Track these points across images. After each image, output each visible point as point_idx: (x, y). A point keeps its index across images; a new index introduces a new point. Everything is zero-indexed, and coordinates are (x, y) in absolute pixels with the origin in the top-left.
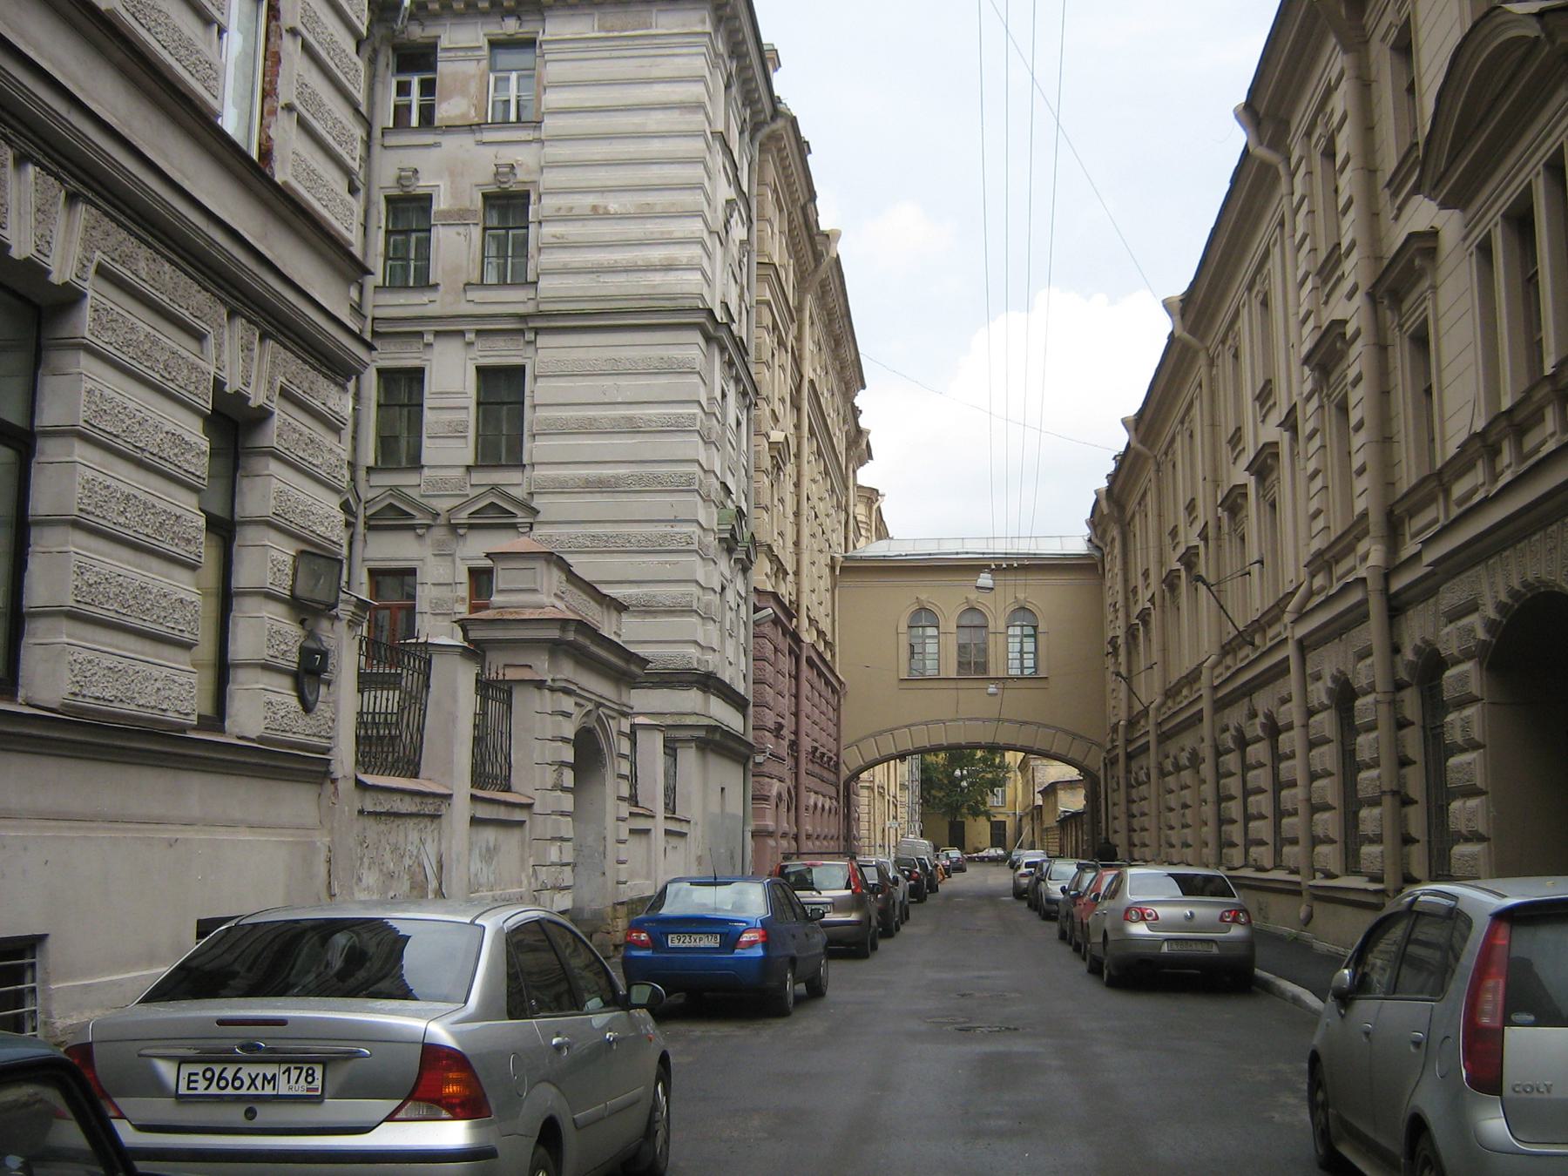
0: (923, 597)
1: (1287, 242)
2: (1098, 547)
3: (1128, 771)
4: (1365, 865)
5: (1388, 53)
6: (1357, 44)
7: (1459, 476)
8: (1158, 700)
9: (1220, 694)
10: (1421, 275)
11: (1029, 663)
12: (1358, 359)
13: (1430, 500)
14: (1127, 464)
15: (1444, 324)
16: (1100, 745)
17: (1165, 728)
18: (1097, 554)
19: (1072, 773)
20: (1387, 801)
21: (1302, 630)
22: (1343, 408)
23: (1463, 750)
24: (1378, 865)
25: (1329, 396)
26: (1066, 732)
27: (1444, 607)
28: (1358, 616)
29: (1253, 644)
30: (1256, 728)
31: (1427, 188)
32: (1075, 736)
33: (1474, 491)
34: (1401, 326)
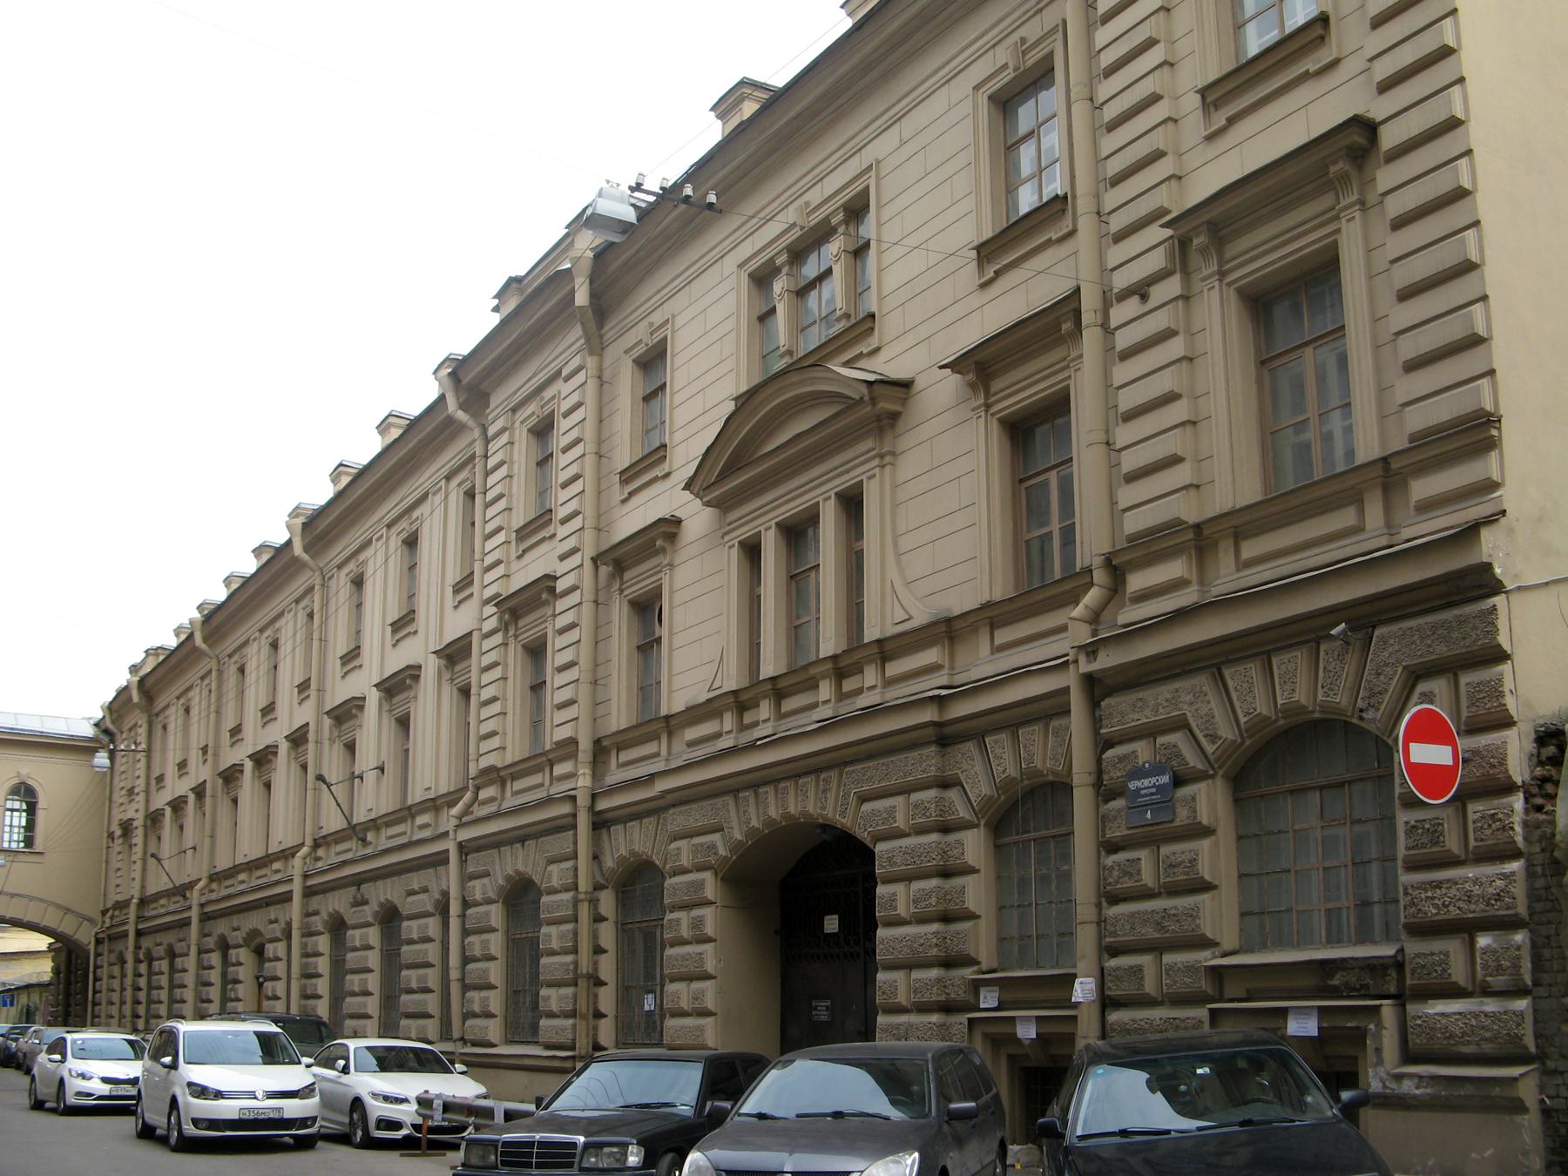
2: (106, 732)
3: (138, 947)
4: (544, 1037)
5: (630, 363)
6: (596, 345)
8: (202, 884)
9: (310, 883)
10: (663, 550)
13: (655, 737)
14: (174, 660)
15: (679, 597)
16: (91, 920)
17: (208, 909)
19: (41, 942)
20: (582, 983)
21: (464, 835)
22: (536, 651)
24: (570, 1036)
25: (516, 636)
26: (58, 906)
28: (568, 825)
29: (364, 840)
30: (160, 951)
32: (68, 910)
34: (621, 591)
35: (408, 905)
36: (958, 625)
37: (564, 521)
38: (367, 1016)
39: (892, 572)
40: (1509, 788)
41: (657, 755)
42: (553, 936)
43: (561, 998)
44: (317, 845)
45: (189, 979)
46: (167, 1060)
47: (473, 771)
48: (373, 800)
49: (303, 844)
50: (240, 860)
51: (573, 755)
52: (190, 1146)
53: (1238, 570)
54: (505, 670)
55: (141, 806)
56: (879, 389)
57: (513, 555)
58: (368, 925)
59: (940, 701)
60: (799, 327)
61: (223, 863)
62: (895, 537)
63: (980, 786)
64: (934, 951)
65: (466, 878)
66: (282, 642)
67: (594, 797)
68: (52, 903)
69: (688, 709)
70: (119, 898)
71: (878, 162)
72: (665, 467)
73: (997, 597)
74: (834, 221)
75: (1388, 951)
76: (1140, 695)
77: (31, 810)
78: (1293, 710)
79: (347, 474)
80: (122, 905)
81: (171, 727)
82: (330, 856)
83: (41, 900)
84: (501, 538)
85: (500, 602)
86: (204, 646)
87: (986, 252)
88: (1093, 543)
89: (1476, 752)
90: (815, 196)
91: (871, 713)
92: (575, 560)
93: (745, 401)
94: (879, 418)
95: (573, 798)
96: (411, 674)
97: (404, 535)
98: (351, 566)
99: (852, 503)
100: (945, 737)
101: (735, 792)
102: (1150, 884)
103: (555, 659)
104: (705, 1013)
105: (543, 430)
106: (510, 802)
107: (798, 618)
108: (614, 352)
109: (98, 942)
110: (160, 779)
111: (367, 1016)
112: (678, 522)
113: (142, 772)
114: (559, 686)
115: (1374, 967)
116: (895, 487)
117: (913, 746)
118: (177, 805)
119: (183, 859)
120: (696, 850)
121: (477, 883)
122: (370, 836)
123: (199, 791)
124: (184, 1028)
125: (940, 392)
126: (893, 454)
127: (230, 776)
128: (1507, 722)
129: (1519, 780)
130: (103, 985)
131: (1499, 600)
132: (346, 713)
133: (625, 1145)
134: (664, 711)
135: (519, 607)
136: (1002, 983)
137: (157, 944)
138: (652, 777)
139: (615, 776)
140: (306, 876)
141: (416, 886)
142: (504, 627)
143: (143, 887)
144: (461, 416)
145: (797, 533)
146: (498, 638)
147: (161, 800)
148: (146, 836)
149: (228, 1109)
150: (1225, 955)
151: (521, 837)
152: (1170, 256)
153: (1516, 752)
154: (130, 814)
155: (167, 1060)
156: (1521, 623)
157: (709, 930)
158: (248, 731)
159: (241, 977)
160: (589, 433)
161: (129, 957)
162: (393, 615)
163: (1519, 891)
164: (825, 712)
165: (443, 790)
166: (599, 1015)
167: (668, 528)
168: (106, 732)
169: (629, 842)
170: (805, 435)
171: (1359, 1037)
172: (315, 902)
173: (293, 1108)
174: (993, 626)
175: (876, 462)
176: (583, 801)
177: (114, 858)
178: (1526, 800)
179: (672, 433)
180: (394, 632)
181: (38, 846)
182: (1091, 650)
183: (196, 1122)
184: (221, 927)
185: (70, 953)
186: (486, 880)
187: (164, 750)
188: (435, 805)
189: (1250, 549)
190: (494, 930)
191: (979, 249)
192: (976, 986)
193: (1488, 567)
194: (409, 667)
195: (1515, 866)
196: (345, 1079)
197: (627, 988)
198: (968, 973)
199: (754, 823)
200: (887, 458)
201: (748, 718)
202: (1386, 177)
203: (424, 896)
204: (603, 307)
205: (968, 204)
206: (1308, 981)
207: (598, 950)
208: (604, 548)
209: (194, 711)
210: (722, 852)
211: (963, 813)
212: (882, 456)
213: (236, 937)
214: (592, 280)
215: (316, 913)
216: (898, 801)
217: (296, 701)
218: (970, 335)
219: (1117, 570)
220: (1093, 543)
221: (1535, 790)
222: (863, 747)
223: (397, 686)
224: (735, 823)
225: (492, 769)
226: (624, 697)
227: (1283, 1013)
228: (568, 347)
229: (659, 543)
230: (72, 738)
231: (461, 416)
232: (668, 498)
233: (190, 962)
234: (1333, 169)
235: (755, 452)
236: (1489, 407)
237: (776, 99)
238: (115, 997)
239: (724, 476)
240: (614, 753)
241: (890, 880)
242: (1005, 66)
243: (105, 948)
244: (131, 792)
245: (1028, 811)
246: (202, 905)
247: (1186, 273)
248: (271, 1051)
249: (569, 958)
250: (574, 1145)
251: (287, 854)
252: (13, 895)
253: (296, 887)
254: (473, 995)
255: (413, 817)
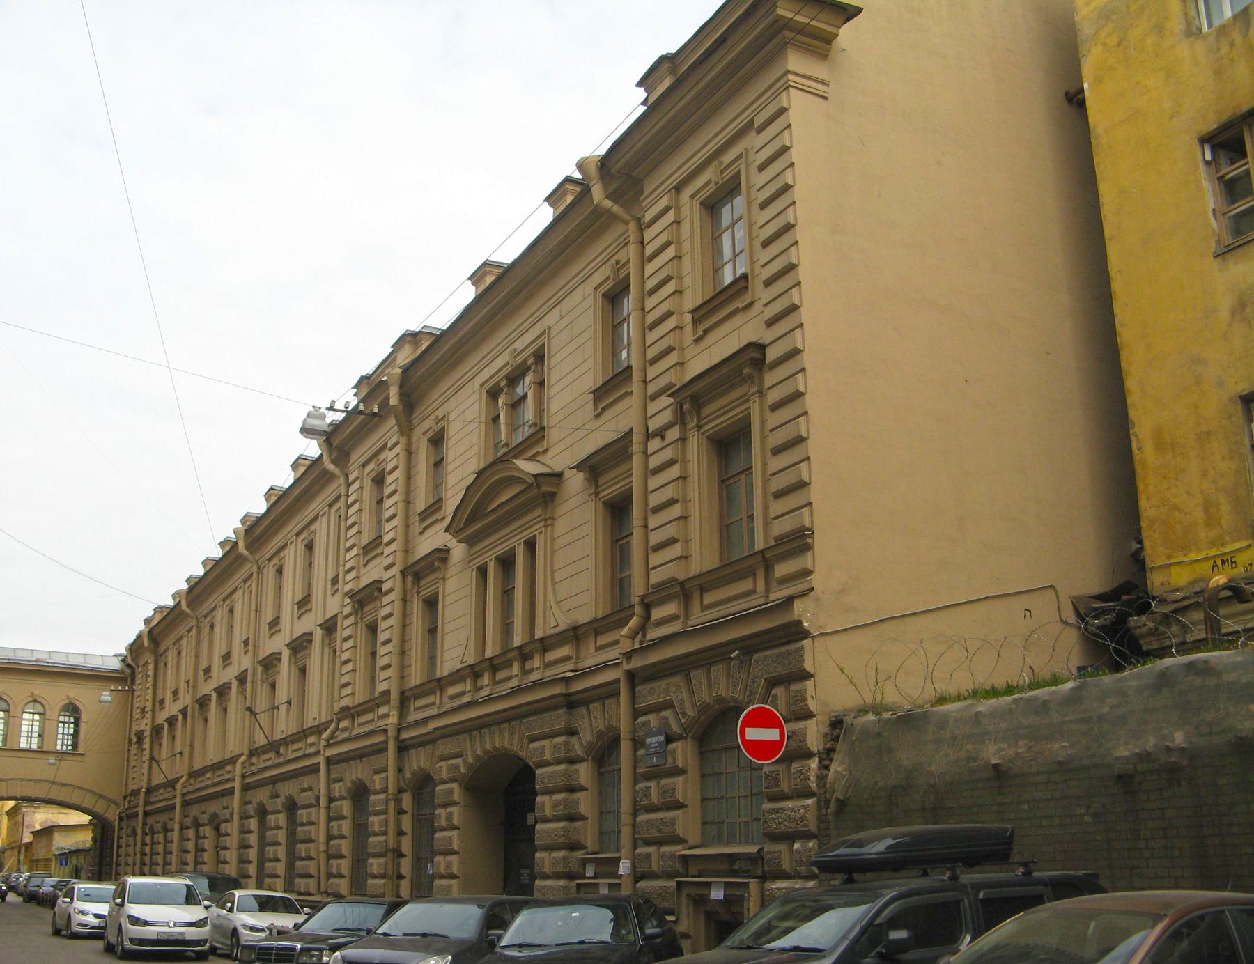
0: (36, 692)
1: (342, 523)
3: (145, 824)
4: (369, 891)
6: (406, 429)
7: (452, 683)
8: (184, 779)
9: (247, 781)
10: (439, 569)
11: (35, 741)
12: (389, 604)
13: (432, 692)
14: (170, 617)
15: (448, 600)
16: (116, 804)
17: (187, 798)
18: (128, 671)
19: (85, 819)
20: (390, 855)
21: (330, 752)
22: (373, 629)
23: (445, 830)
26: (93, 793)
27: (438, 753)
28: (381, 749)
29: (278, 752)
30: (158, 827)
31: (452, 530)
32: (100, 796)
33: (463, 693)
34: (418, 593)
35: (304, 798)
36: (580, 632)
37: (388, 544)
38: (277, 876)
39: (550, 596)
40: (810, 755)
41: (753, 592)
42: (375, 822)
43: (379, 865)
44: (252, 754)
45: (174, 847)
46: (119, 901)
47: (336, 709)
48: (285, 725)
49: (242, 754)
50: (208, 763)
51: (387, 702)
52: (127, 955)
53: (702, 611)
54: (355, 642)
55: (149, 721)
56: (540, 479)
57: (362, 564)
58: (279, 812)
59: (567, 680)
60: (513, 429)
61: (198, 765)
62: (553, 572)
63: (587, 736)
64: (562, 840)
65: (330, 781)
66: (453, 430)
67: (399, 731)
68: (90, 791)
69: (450, 675)
70: (134, 787)
71: (549, 328)
72: (747, 298)
73: (600, 615)
74: (529, 362)
75: (753, 849)
76: (653, 685)
77: (77, 723)
78: (719, 700)
79: (571, 191)
80: (135, 793)
81: (169, 666)
82: (260, 763)
83: (82, 789)
84: (354, 552)
85: (351, 595)
86: (187, 610)
87: (600, 393)
88: (637, 589)
89: (793, 732)
90: (519, 345)
91: (537, 684)
92: (394, 571)
93: (480, 474)
94: (544, 495)
95: (386, 731)
96: (307, 639)
97: (306, 542)
98: (275, 561)
99: (531, 545)
100: (572, 703)
101: (469, 731)
102: (786, 790)
103: (382, 637)
104: (453, 877)
105: (379, 481)
106: (698, 617)
107: (621, 571)
108: (418, 432)
109: (121, 819)
110: (162, 702)
111: (277, 876)
112: (448, 551)
113: (150, 697)
114: (386, 653)
115: (750, 858)
116: (553, 540)
117: (556, 707)
118: (171, 721)
119: (172, 765)
120: (449, 769)
121: (337, 785)
122: (282, 750)
123: (184, 712)
124: (131, 880)
125: (575, 482)
126: (553, 519)
127: (203, 703)
128: (810, 715)
129: (815, 750)
130: (122, 851)
131: (804, 642)
132: (270, 663)
133: (321, 950)
134: (438, 676)
135: (365, 598)
136: (598, 862)
137: (156, 822)
138: (427, 719)
139: (413, 716)
140: (244, 777)
141: (306, 786)
142: (355, 612)
143: (149, 780)
144: (331, 467)
145: (506, 563)
146: (351, 620)
147: (162, 717)
148: (152, 743)
149: (151, 932)
150: (691, 848)
151: (360, 755)
152: (674, 413)
153: (814, 733)
154: (142, 727)
155: (119, 901)
156: (813, 655)
157: (456, 822)
158: (215, 671)
159: (206, 847)
160: (401, 489)
161: (139, 831)
162: (298, 597)
163: (812, 818)
164: (514, 683)
165: (323, 720)
166: (400, 877)
167: (442, 555)
168: (129, 666)
169: (418, 760)
170: (505, 505)
171: (740, 900)
172: (249, 795)
173: (192, 933)
174: (597, 633)
175: (542, 524)
176: (392, 733)
177: (132, 758)
178: (820, 761)
179: (549, 417)
180: (299, 608)
181: (81, 750)
182: (628, 656)
183: (131, 940)
184: (194, 811)
185: (103, 827)
186: (341, 784)
187: (165, 681)
188: (318, 730)
189: (709, 598)
190: (345, 818)
191: (594, 392)
192: (584, 862)
193: (800, 623)
194: (304, 634)
195: (810, 801)
196: (231, 916)
197: (419, 859)
198: (579, 854)
199: (479, 752)
200: (550, 521)
201: (528, 666)
202: (770, 378)
203: (309, 793)
204: (410, 401)
205: (590, 363)
206: (724, 866)
207: (401, 833)
208: (410, 562)
209: (184, 653)
210: (463, 770)
211: (579, 752)
212: (546, 520)
213: (204, 818)
214: (401, 386)
215: (250, 803)
216: (546, 742)
217: (329, 592)
218: (590, 447)
219: (648, 607)
220: (637, 589)
221: (824, 756)
222: (535, 706)
223: (299, 646)
224: (469, 753)
225: (346, 708)
226: (419, 664)
227: (708, 885)
228: (389, 431)
229: (436, 564)
230: (106, 670)
231: (331, 467)
232: (435, 538)
233: (175, 835)
234: (745, 371)
235: (488, 505)
236: (808, 525)
237: (507, 271)
238: (130, 860)
239: (471, 520)
240: (697, 595)
241: (543, 794)
242: (608, 278)
243: (124, 825)
244: (143, 710)
245: (604, 752)
246: (183, 795)
247: (683, 424)
248: (191, 898)
249: (382, 838)
250: (294, 949)
251: (233, 761)
252: (62, 785)
253: (237, 785)
254: (334, 862)
255: (442, 690)
